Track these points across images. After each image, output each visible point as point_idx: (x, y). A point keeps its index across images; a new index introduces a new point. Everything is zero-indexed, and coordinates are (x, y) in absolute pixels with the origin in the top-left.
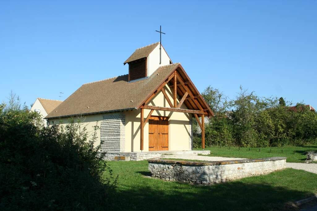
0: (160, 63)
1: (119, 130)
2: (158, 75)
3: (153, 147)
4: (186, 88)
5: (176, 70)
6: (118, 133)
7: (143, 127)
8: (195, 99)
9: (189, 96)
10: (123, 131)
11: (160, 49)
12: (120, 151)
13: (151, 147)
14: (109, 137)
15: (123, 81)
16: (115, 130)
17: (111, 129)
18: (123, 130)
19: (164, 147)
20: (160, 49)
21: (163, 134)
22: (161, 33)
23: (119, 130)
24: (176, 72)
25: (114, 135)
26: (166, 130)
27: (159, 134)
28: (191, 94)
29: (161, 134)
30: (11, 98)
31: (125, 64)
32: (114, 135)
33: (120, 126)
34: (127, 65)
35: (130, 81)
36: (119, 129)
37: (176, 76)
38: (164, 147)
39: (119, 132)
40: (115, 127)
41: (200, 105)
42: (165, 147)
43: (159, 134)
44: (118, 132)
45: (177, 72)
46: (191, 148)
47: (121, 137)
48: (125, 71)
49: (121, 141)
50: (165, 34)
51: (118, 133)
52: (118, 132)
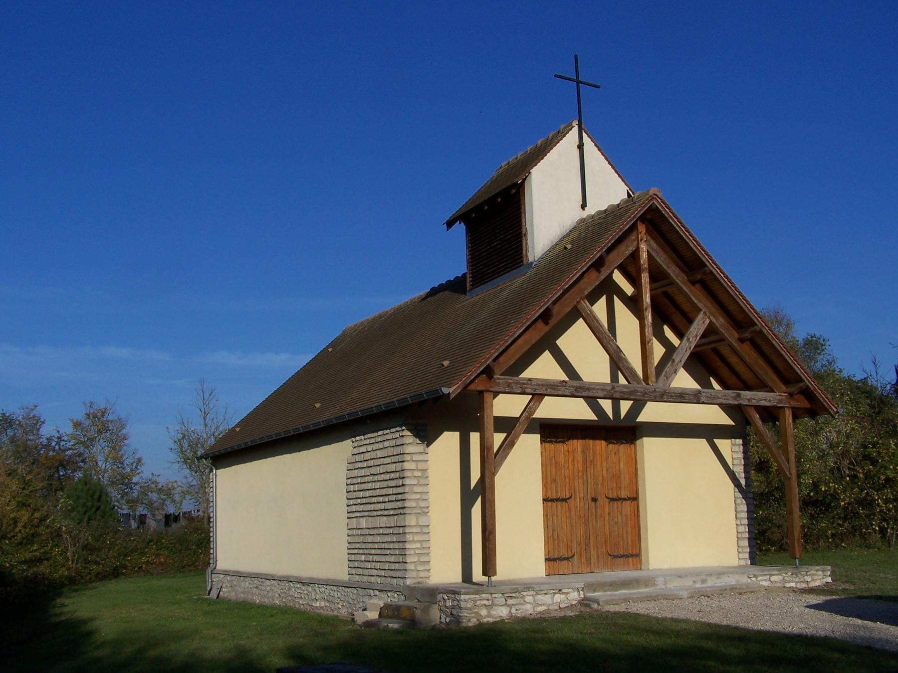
0: (584, 206)
1: (400, 490)
2: (566, 248)
3: (567, 559)
4: (697, 296)
5: (642, 219)
6: (400, 504)
7: (494, 474)
8: (742, 341)
9: (710, 331)
10: (418, 496)
11: (581, 147)
12: (408, 582)
13: (559, 559)
14: (372, 522)
15: (447, 292)
16: (390, 491)
17: (378, 485)
18: (416, 489)
19: (622, 556)
20: (581, 147)
21: (612, 500)
22: (578, 82)
23: (400, 490)
24: (642, 228)
25: (386, 513)
26: (625, 481)
27: (594, 500)
28: (720, 322)
29: (602, 501)
30: (201, 403)
31: (450, 224)
32: (386, 513)
33: (407, 474)
34: (460, 228)
35: (471, 290)
36: (403, 485)
37: (643, 247)
38: (622, 556)
39: (400, 497)
40: (387, 476)
41: (762, 362)
42: (627, 556)
43: (594, 500)
44: (399, 497)
45: (648, 232)
46: (747, 556)
47: (411, 520)
48: (452, 257)
49: (409, 537)
50: (576, 57)
51: (400, 504)
52: (399, 497)
